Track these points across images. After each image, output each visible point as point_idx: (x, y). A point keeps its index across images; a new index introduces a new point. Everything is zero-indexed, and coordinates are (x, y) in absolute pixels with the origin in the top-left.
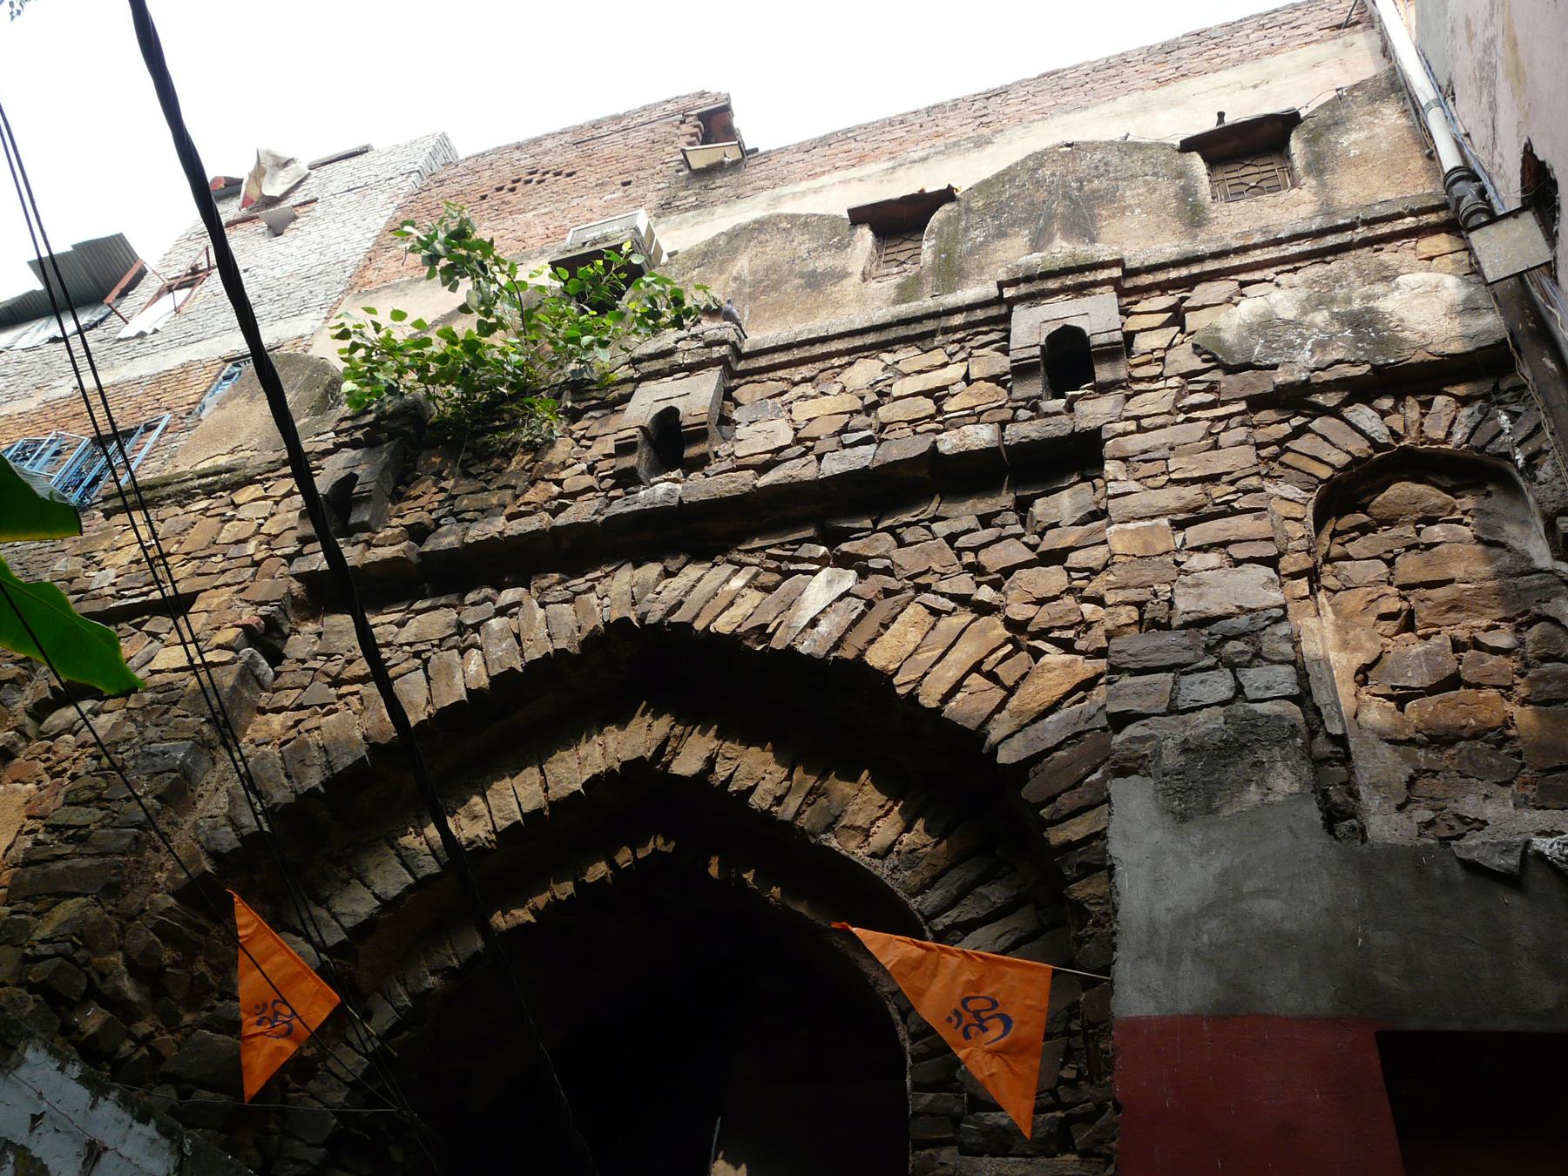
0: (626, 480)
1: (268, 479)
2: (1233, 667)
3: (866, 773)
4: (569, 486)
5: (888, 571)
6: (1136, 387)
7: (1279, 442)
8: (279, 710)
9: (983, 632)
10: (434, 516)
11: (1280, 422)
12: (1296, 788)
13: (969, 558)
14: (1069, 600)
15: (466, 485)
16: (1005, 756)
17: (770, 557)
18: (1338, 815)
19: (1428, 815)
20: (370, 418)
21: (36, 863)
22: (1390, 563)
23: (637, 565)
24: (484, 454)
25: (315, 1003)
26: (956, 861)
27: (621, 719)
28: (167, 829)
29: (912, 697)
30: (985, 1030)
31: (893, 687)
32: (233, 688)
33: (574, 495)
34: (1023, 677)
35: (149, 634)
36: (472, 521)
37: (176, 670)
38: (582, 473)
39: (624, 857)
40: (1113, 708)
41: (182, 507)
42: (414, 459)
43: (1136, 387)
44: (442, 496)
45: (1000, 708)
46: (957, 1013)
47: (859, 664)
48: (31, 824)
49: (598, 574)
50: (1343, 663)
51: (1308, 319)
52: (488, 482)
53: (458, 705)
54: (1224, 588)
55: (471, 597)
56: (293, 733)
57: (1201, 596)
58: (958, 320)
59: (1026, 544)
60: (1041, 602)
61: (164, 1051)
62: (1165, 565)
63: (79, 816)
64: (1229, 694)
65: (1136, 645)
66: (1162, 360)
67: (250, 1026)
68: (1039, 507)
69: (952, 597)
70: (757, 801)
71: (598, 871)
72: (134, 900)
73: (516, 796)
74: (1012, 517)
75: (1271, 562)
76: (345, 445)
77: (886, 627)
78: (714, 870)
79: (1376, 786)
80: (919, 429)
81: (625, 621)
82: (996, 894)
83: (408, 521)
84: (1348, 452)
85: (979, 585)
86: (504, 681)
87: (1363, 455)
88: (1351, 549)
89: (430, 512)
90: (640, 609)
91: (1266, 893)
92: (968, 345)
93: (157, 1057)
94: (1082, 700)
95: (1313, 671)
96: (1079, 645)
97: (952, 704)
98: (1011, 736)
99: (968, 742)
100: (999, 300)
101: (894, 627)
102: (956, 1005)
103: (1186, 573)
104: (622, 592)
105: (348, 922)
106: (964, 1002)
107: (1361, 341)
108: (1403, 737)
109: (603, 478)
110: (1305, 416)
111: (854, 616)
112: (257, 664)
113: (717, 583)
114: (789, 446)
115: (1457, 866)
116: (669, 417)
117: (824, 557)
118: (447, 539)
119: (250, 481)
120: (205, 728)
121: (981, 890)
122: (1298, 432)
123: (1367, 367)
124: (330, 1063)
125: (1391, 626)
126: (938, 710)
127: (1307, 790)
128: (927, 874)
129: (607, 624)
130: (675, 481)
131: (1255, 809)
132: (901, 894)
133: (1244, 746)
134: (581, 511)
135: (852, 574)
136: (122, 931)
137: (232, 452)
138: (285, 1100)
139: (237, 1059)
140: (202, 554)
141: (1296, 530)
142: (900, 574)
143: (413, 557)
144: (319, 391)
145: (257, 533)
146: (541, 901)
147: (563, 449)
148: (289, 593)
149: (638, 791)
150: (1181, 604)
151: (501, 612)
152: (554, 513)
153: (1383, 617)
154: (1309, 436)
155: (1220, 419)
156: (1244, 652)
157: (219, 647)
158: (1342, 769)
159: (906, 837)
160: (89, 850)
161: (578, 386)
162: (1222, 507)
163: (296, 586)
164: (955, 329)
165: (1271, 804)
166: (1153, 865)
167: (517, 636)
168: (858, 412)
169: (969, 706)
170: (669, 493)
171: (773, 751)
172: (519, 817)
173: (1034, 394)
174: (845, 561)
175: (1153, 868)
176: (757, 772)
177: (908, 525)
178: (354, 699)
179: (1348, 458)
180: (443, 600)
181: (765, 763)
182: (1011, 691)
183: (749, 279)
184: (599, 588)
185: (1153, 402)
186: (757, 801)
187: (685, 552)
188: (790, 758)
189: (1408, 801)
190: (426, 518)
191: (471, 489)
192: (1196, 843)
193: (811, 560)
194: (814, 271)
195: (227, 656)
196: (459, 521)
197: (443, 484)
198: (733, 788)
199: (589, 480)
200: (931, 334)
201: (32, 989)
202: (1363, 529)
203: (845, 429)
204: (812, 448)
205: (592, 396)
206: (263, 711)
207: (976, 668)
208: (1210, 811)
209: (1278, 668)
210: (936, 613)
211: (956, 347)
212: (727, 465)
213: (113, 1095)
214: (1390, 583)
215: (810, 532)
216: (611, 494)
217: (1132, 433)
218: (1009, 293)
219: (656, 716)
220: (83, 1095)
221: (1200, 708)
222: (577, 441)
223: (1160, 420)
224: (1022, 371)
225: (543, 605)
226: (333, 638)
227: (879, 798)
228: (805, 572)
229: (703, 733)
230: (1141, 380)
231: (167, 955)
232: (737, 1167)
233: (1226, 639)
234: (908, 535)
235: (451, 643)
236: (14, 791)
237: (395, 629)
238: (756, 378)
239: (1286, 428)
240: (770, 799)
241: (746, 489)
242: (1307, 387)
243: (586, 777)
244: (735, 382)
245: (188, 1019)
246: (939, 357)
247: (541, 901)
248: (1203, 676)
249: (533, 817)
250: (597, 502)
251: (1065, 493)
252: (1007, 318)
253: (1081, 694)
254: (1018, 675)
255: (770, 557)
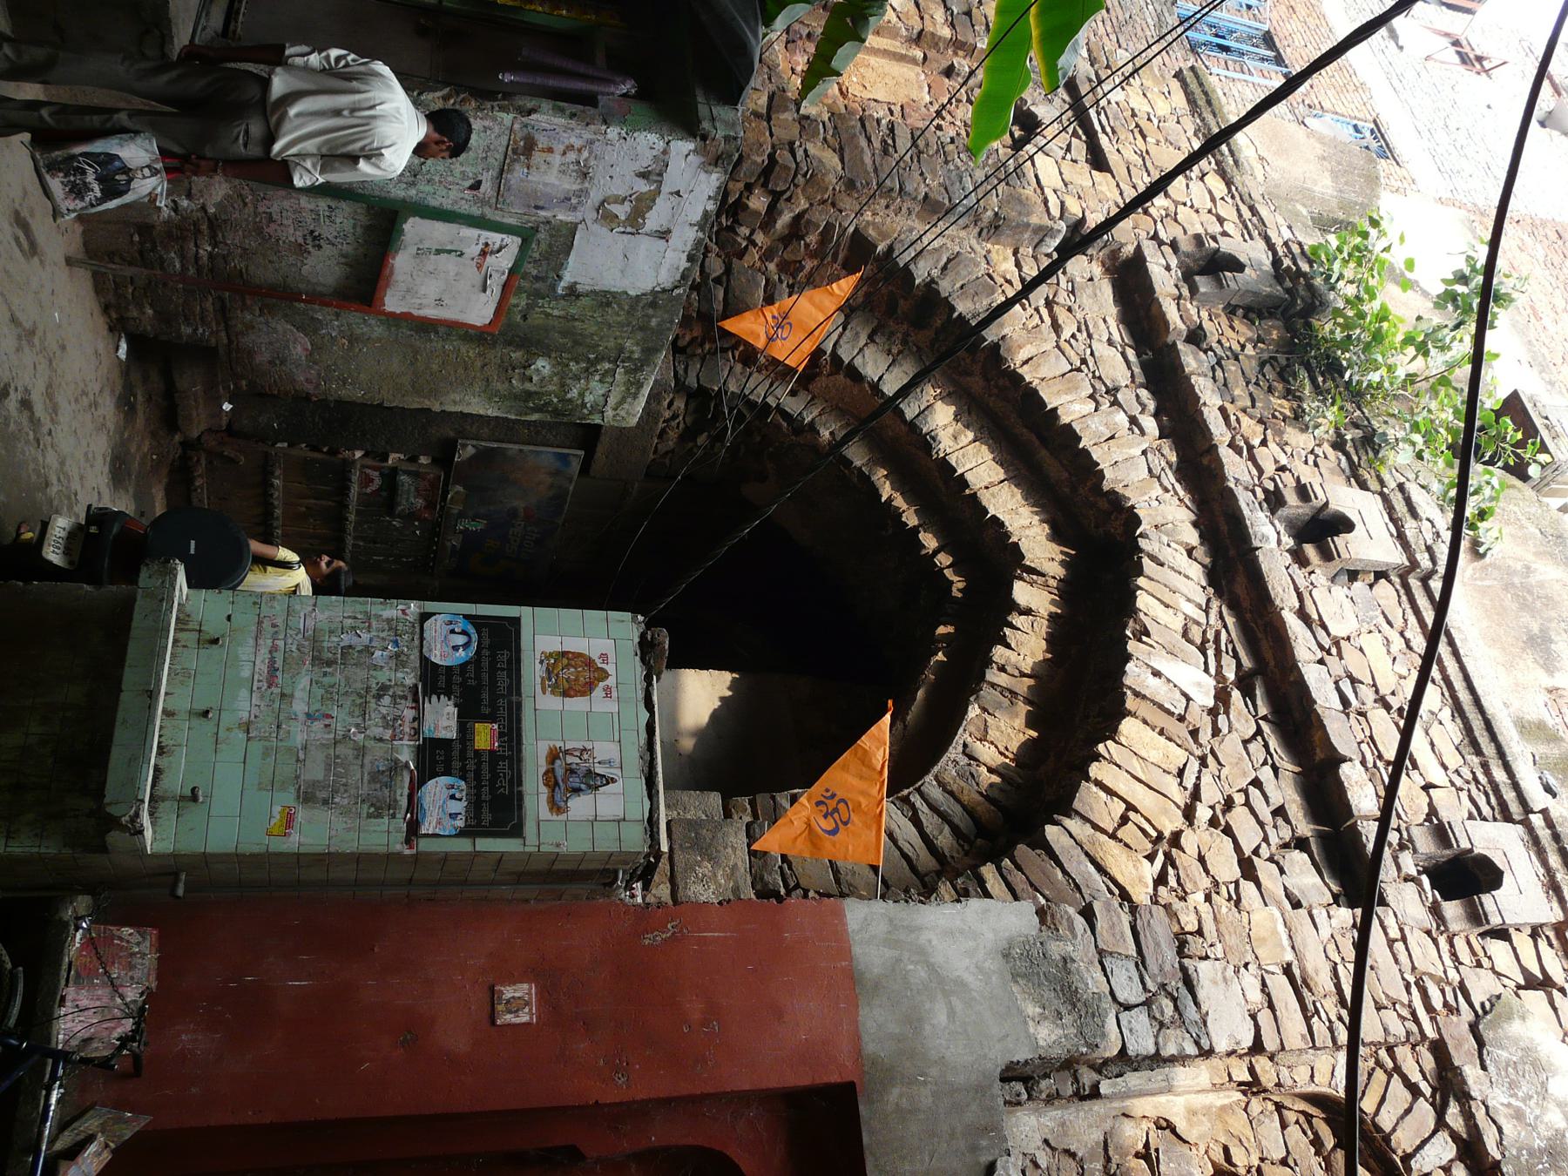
0: (1274, 500)
1: (1233, 197)
2: (1147, 1003)
3: (1035, 734)
4: (1260, 453)
5: (1216, 732)
6: (1442, 940)
7: (1397, 1069)
8: (1018, 265)
9: (1165, 811)
10: (1214, 345)
11: (1422, 1071)
12: (1042, 1043)
13: (1239, 799)
14: (1206, 882)
15: (1251, 367)
16: (1051, 831)
17: (1218, 634)
18: (1024, 1078)
19: (1043, 1163)
20: (1305, 267)
21: (863, 126)
22: (1284, 1162)
23: (1195, 524)
24: (1284, 374)
25: (792, 351)
26: (968, 810)
27: (1057, 536)
28: (904, 210)
29: (1097, 757)
30: (825, 817)
31: (1104, 740)
32: (1028, 225)
33: (1252, 458)
34: (1126, 845)
35: (1069, 146)
36: (1214, 378)
37: (1036, 176)
38: (1276, 462)
39: (944, 560)
40: (1097, 906)
41: (1195, 134)
42: (1271, 316)
43: (1442, 940)
44: (1236, 347)
45: (1096, 827)
46: (833, 796)
47: (1119, 712)
48: (897, 110)
49: (1181, 493)
50: (1174, 1107)
51: (1552, 1106)
52: (1257, 384)
53: (1043, 404)
54: (1227, 1009)
55: (1144, 393)
56: (1000, 281)
57: (1215, 983)
58: (1500, 775)
59: (1258, 847)
60: (1202, 859)
61: (746, 258)
62: (1243, 954)
63: (903, 142)
64: (1121, 997)
65: (1159, 931)
66: (1479, 965)
67: (770, 312)
68: (1298, 858)
69: (1197, 787)
70: (999, 653)
71: (929, 541)
72: (848, 204)
73: (977, 465)
74: (1286, 834)
75: (1257, 1047)
76: (1275, 253)
77: (1161, 733)
78: (942, 630)
79: (1063, 1124)
80: (1364, 747)
81: (1138, 522)
82: (945, 839)
83: (1207, 325)
84: (1394, 1130)
85: (1212, 807)
86: (1069, 435)
87: (1393, 1144)
88: (1294, 1130)
89: (1219, 342)
90: (1152, 533)
91: (952, 1014)
92: (1473, 787)
93: (741, 254)
94: (1111, 892)
95: (1159, 1074)
96: (1162, 889)
97: (1094, 789)
98: (1071, 836)
99: (1063, 805)
100: (1527, 809)
101: (1162, 739)
102: (840, 794)
103: (1237, 971)
104: (1167, 520)
105: (858, 362)
106: (842, 800)
107: (1530, 1154)
108: (1111, 1153)
109: (1273, 480)
110: (1433, 1095)
111: (1167, 705)
112: (1053, 237)
113: (1186, 591)
114: (1329, 634)
115: (991, 1158)
116: (1343, 524)
117: (1224, 678)
118: (1190, 359)
119: (1229, 183)
120: (990, 213)
121: (947, 829)
122: (1415, 1091)
123: (1498, 1157)
124: (755, 375)
125: (1219, 1157)
126: (1088, 779)
127: (1041, 1052)
128: (955, 787)
129: (1133, 507)
130: (1279, 542)
131: (1020, 1011)
132: (936, 769)
133: (1074, 1006)
134: (1235, 468)
135: (1211, 703)
136: (824, 202)
137: (1261, 158)
138: (724, 350)
139: (748, 309)
140: (1149, 164)
141: (1302, 1074)
142: (1215, 742)
143: (1170, 339)
144: (1341, 215)
145: (1176, 203)
146: (899, 502)
147: (1299, 440)
148: (1122, 245)
149: (995, 559)
150: (1203, 966)
151: (1133, 421)
152: (1232, 445)
153: (1226, 1150)
154: (1409, 1097)
155: (1414, 1014)
156: (1162, 1013)
157: (1062, 203)
158: (1070, 1092)
159: (983, 769)
160: (878, 159)
161: (1370, 441)
162: (1311, 1007)
163: (1129, 250)
164: (1487, 773)
165: (1026, 1023)
166: (970, 934)
167: (1112, 437)
168: (1377, 692)
169: (1089, 798)
170: (1265, 538)
171: (1045, 660)
172: (960, 471)
173: (1418, 845)
174: (1222, 696)
175: (962, 932)
176: (1025, 646)
177: (1266, 746)
178: (1036, 320)
179: (1387, 1129)
180: (1137, 370)
181: (1033, 654)
182: (1113, 836)
183: (1533, 580)
184: (1168, 495)
185: (1426, 955)
186: (999, 653)
187: (1214, 563)
188: (1042, 675)
189: (1053, 1149)
190: (1212, 340)
191: (1247, 371)
192: (987, 965)
193: (1219, 667)
194: (1551, 641)
195: (1056, 212)
196: (1213, 369)
197: (1249, 346)
198: (1007, 631)
199: (1269, 468)
200: (1478, 751)
201: (771, 157)
202: (1317, 1142)
203: (1354, 681)
204: (1329, 653)
205: (1361, 451)
206: (1015, 253)
207: (1130, 807)
208: (1015, 977)
209: (1151, 1041)
210: (1181, 773)
211: (1469, 777)
212: (1302, 584)
213: (700, 235)
214: (1262, 1160)
215: (1247, 663)
216: (1258, 490)
217: (1386, 934)
218: (1537, 820)
219: (1062, 563)
220: (697, 216)
221: (1106, 975)
222: (1312, 452)
223: (1403, 957)
224: (1441, 833)
225: (1144, 453)
226: (1089, 291)
227: (1014, 746)
228: (1206, 663)
229: (1053, 602)
230: (1452, 945)
231: (812, 239)
232: (729, 688)
233: (1175, 1000)
234: (1256, 747)
235: (1098, 385)
236: (921, 88)
237: (1105, 338)
238: (1404, 598)
239: (1416, 1077)
240: (1002, 662)
241: (1278, 602)
242: (1464, 1097)
243: (1000, 516)
244: (1396, 580)
245: (772, 267)
246: (1453, 760)
247: (899, 502)
248: (1136, 979)
249: (962, 482)
250: (1247, 478)
251: (1318, 879)
252: (1507, 817)
253: (1117, 892)
254: (1128, 841)
255: (1218, 634)
